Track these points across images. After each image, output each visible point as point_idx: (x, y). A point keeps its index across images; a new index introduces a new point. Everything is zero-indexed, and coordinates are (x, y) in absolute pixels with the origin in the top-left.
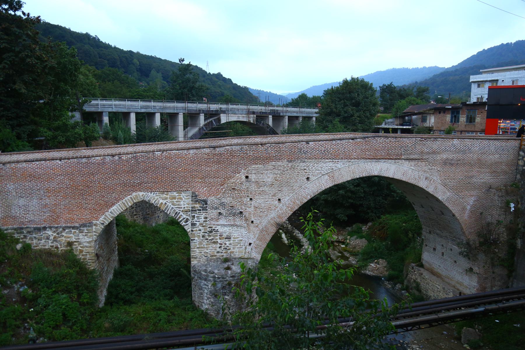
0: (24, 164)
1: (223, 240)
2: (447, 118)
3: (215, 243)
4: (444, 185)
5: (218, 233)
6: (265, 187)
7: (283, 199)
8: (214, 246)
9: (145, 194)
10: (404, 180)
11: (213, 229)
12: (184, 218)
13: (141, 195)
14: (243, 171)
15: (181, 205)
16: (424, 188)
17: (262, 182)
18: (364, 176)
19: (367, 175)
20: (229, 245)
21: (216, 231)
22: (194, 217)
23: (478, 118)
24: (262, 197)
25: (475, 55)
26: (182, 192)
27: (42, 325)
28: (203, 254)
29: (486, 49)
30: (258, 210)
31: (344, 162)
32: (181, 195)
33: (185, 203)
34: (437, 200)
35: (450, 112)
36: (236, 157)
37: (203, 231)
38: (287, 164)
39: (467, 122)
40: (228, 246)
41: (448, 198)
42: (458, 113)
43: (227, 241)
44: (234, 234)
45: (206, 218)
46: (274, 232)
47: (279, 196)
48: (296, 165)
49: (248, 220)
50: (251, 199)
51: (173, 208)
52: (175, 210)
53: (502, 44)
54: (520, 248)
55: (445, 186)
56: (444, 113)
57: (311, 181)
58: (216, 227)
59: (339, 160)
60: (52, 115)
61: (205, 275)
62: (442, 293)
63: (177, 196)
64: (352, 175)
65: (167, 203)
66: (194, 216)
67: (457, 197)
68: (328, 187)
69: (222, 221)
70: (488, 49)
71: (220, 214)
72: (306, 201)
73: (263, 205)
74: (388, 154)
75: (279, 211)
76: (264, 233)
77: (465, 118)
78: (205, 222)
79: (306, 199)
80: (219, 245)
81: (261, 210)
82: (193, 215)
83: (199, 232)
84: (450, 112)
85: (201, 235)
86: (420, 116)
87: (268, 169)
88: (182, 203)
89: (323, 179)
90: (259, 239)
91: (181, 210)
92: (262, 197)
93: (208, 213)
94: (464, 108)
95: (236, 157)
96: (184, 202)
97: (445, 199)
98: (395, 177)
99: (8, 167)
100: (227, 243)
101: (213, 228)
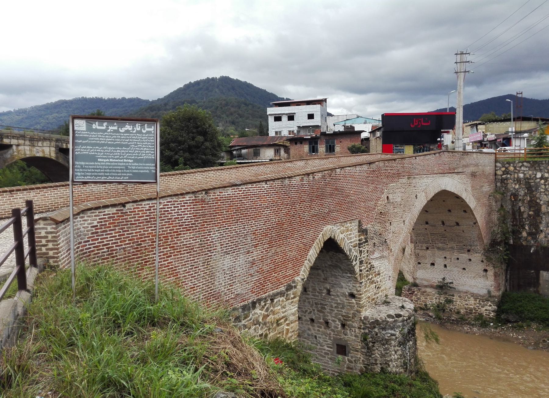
0: (230, 191)
2: (305, 149)
23: (338, 148)
25: (181, 88)
29: (192, 82)
35: (308, 142)
39: (327, 151)
42: (317, 143)
53: (208, 78)
54: (512, 243)
56: (301, 143)
61: (392, 323)
62: (459, 302)
70: (194, 82)
74: (450, 169)
77: (325, 148)
84: (308, 142)
86: (251, 150)
94: (323, 137)
99: (212, 197)
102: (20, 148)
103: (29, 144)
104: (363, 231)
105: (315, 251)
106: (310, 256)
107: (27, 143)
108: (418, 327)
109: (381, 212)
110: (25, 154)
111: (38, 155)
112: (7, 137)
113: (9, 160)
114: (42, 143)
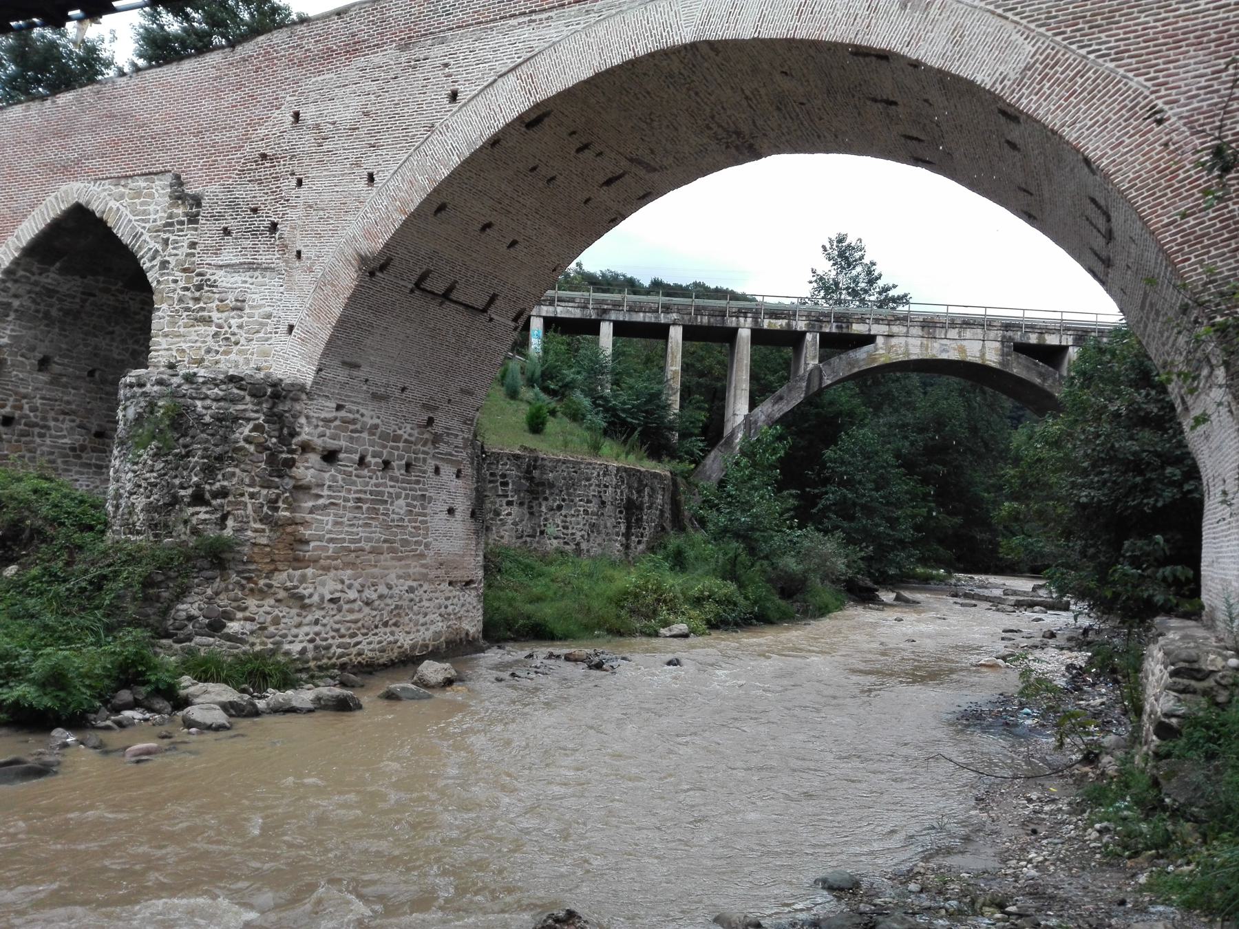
1: (226, 313)
3: (207, 321)
4: (1000, 11)
5: (215, 290)
6: (337, 138)
7: (380, 174)
8: (202, 329)
9: (82, 185)
10: (802, 34)
11: (205, 278)
12: (150, 249)
13: (74, 191)
14: (288, 99)
15: (149, 214)
16: (898, 49)
17: (329, 126)
18: (641, 53)
19: (652, 47)
20: (236, 331)
21: (210, 286)
22: (166, 242)
24: (325, 173)
26: (156, 177)
27: (456, 819)
28: (175, 354)
30: (314, 213)
31: (570, 16)
32: (153, 185)
33: (159, 208)
34: (966, 88)
36: (276, 61)
37: (182, 284)
38: (397, 58)
40: (234, 334)
41: (1027, 68)
43: (233, 317)
44: (254, 296)
45: (193, 245)
46: (351, 287)
47: (369, 165)
48: (422, 57)
49: (286, 247)
50: (300, 183)
51: (130, 221)
52: (133, 228)
55: (1009, 14)
57: (463, 101)
58: (214, 274)
59: (550, 14)
60: (1174, 897)
63: (144, 188)
64: (598, 59)
65: (121, 207)
66: (168, 239)
67: (1083, 52)
68: (516, 114)
69: (229, 256)
71: (227, 232)
72: (446, 173)
73: (326, 197)
75: (369, 215)
76: (328, 290)
78: (188, 258)
79: (445, 166)
80: (214, 329)
81: (321, 213)
82: (165, 236)
83: (172, 285)
85: (176, 296)
87: (347, 82)
88: (152, 208)
89: (501, 91)
90: (316, 312)
91: (147, 225)
92: (325, 173)
93: (199, 232)
95: (276, 61)
96: (156, 204)
97: (1012, 76)
98: (765, 35)
100: (232, 321)
101: (208, 276)
102: (894, 341)
103: (920, 333)
104: (179, 195)
105: (34, 224)
106: (22, 230)
107: (916, 331)
108: (230, 517)
109: (264, 156)
110: (907, 353)
111: (944, 356)
112: (862, 320)
113: (862, 363)
114: (960, 332)
